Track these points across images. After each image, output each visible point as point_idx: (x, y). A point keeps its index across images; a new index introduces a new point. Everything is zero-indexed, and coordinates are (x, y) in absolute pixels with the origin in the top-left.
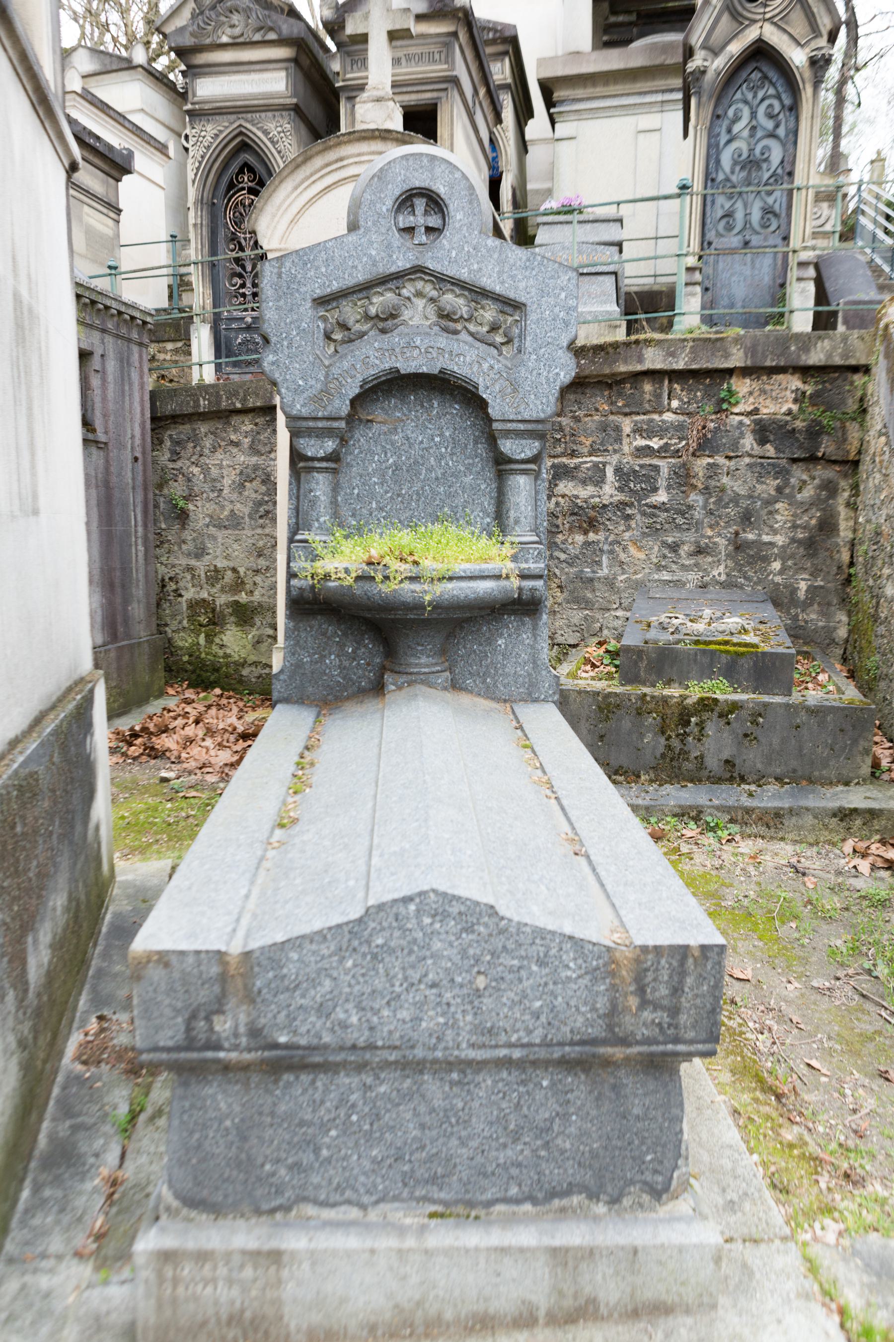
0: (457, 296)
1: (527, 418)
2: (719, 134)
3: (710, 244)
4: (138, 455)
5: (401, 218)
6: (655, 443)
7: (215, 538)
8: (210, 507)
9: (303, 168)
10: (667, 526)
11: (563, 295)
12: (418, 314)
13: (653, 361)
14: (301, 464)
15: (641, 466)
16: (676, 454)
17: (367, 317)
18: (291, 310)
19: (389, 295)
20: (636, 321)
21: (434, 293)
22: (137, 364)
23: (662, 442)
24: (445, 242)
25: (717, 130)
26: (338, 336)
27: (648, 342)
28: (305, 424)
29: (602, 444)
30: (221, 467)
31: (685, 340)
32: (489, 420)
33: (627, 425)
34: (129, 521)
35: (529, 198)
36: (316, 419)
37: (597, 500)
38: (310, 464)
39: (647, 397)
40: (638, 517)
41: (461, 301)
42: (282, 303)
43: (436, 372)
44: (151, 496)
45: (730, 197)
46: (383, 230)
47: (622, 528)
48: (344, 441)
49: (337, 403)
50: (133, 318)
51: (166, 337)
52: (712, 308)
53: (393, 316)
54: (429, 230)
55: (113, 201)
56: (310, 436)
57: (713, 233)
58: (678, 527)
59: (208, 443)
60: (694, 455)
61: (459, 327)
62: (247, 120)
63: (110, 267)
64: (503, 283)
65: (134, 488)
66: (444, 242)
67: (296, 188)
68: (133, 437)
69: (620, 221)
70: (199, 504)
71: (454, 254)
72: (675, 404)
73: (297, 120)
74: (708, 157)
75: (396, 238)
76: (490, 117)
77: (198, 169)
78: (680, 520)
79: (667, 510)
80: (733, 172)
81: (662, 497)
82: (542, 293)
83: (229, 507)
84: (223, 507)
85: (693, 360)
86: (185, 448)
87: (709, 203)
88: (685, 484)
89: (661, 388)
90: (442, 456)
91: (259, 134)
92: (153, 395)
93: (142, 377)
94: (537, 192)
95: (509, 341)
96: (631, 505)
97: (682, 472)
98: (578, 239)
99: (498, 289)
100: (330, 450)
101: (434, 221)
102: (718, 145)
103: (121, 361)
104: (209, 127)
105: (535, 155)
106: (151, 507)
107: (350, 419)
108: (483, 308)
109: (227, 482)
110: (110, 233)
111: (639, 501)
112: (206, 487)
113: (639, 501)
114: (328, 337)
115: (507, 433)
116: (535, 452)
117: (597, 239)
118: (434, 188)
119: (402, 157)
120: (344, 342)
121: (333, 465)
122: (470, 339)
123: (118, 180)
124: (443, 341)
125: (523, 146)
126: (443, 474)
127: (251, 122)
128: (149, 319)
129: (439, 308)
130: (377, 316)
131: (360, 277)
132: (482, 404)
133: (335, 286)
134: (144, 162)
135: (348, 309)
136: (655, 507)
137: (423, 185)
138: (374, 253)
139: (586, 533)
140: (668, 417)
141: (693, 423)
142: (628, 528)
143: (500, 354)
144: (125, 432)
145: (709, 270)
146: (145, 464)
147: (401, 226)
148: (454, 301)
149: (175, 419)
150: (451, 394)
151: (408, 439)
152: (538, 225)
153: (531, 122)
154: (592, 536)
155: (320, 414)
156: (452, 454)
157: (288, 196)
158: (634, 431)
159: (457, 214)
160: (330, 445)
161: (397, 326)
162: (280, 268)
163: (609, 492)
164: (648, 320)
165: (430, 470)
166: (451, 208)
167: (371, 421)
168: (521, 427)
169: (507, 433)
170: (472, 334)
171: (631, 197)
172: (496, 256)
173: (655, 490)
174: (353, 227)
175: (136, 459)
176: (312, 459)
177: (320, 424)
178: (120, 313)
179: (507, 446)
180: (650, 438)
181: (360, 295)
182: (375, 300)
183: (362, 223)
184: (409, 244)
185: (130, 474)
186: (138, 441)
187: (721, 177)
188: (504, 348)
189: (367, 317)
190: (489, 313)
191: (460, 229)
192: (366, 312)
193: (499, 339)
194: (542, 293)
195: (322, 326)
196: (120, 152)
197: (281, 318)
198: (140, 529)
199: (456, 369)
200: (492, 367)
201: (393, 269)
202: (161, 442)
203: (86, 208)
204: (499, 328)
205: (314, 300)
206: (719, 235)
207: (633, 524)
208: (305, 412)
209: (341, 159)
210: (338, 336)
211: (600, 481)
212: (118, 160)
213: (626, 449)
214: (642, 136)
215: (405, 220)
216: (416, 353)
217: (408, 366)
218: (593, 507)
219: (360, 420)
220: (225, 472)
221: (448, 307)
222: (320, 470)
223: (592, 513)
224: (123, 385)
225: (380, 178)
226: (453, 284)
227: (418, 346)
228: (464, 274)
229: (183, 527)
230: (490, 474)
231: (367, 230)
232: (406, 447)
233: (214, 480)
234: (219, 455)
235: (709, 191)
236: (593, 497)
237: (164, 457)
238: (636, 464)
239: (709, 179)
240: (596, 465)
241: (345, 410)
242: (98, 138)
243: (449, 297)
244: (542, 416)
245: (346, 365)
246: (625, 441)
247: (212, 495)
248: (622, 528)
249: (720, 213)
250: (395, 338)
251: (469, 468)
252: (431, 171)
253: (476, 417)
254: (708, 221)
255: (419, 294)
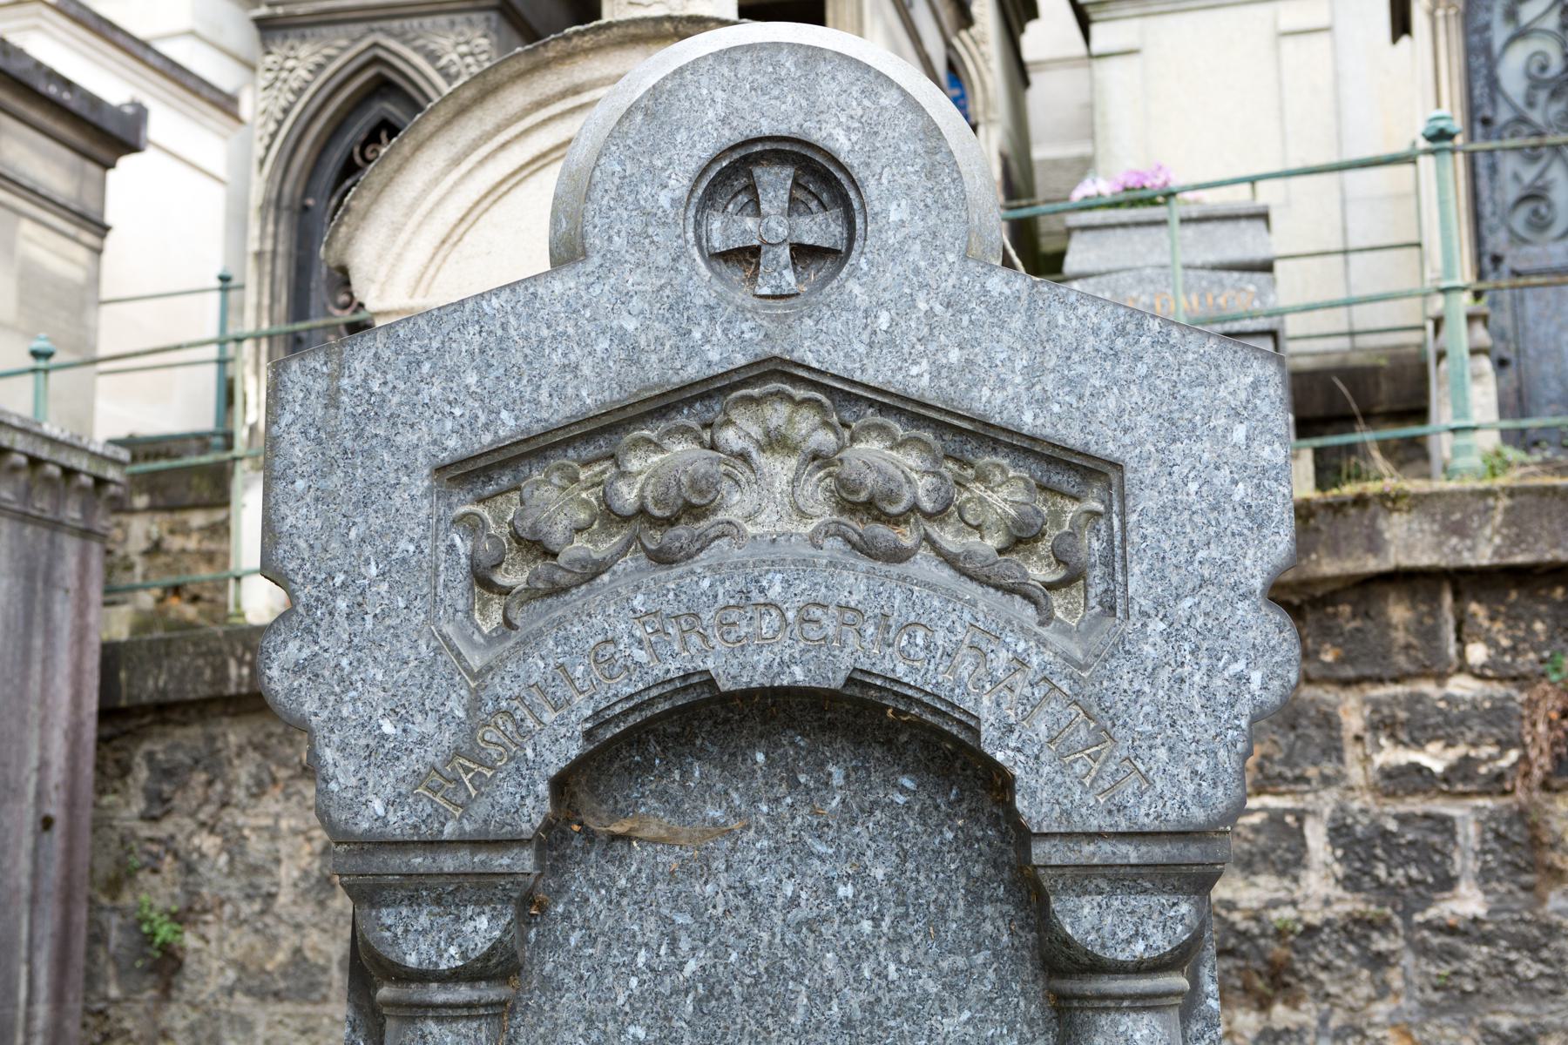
0: (898, 445)
1: (1149, 824)
2: (1487, 27)
3: (1497, 260)
4: (55, 810)
5: (716, 224)
6: (1435, 758)
7: (247, 1026)
8: (241, 941)
9: (478, 113)
10: (1491, 984)
11: (1240, 433)
12: (773, 502)
13: (1409, 549)
14: (385, 992)
15: (1403, 819)
16: (1497, 784)
17: (610, 516)
18: (365, 502)
19: (682, 449)
20: (1351, 449)
21: (825, 439)
22: (71, 582)
23: (1453, 755)
24: (854, 287)
25: (1482, 17)
26: (513, 577)
27: (1390, 501)
28: (396, 862)
29: (1288, 761)
30: (274, 834)
31: (1487, 493)
32: (1021, 836)
33: (1352, 712)
34: (12, 992)
35: (1039, 178)
36: (435, 844)
37: (1288, 913)
38: (415, 993)
39: (1400, 637)
40: (1408, 959)
41: (911, 460)
42: (337, 479)
43: (837, 682)
44: (81, 915)
45: (1531, 155)
46: (662, 259)
47: (1365, 990)
48: (529, 905)
49: (507, 792)
50: (69, 473)
51: (191, 498)
52: (1524, 413)
53: (692, 512)
54: (803, 254)
55: (91, 207)
56: (413, 900)
57: (1502, 236)
58: (1524, 986)
59: (244, 772)
60: (1545, 786)
61: (907, 537)
62: (390, 34)
63: (36, 354)
64: (1042, 402)
65: (33, 900)
66: (853, 286)
67: (456, 162)
68: (43, 766)
69: (1263, 216)
70: (212, 932)
71: (884, 321)
72: (1477, 653)
73: (506, 29)
74: (1469, 74)
75: (702, 281)
76: (947, 14)
77: (273, 136)
78: (1528, 968)
79: (1487, 940)
80: (1531, 104)
81: (1468, 902)
82: (1172, 429)
83: (289, 941)
84: (273, 942)
85: (1516, 542)
86: (184, 786)
87: (1483, 171)
88: (1532, 867)
89: (1435, 612)
90: (865, 948)
91: (418, 60)
92: (112, 655)
93: (82, 612)
94: (1056, 164)
95: (1073, 578)
96: (1385, 926)
97: (1517, 833)
98: (1182, 259)
99: (1028, 421)
100: (483, 946)
101: (818, 228)
102: (1487, 49)
103: (30, 576)
104: (304, 50)
105: (1042, 91)
106: (80, 945)
107: (552, 841)
108: (982, 477)
109: (287, 873)
110: (77, 274)
111: (1406, 915)
112: (233, 888)
113: (1406, 915)
114: (482, 579)
115: (1083, 877)
116: (1181, 933)
117: (1213, 258)
118: (816, 137)
119: (719, 56)
120: (532, 594)
121: (490, 992)
122: (945, 574)
123: (107, 166)
124: (855, 583)
125: (1019, 72)
126: (869, 1008)
127: (401, 36)
128: (112, 473)
129: (842, 483)
130: (642, 511)
131: (589, 397)
132: (998, 783)
133: (508, 425)
134: (168, 122)
135: (549, 493)
136: (1451, 930)
137: (783, 130)
138: (631, 325)
139: (1264, 1005)
140: (1462, 687)
141: (1532, 704)
142: (1383, 991)
143: (1046, 619)
144: (22, 755)
145: (1504, 319)
146: (71, 835)
147: (718, 244)
148: (889, 460)
149: (166, 712)
150: (889, 744)
151: (747, 893)
152: (1069, 232)
153: (1032, 28)
154: (1281, 1014)
155: (449, 830)
156: (896, 940)
157: (436, 181)
158: (1374, 727)
159: (891, 206)
160: (482, 929)
161: (706, 542)
162: (334, 377)
163: (1319, 889)
164: (1386, 448)
165: (823, 994)
166: (871, 190)
167: (626, 838)
168: (1131, 853)
169: (1083, 877)
170: (949, 560)
171: (1333, 159)
172: (1017, 323)
173: (1447, 883)
174: (567, 252)
175: (47, 823)
176: (422, 976)
177: (448, 862)
178: (35, 462)
179: (1085, 918)
180: (1417, 744)
181: (589, 451)
182: (634, 464)
183: (595, 240)
184: (742, 296)
185: (25, 864)
186: (56, 775)
187: (1504, 115)
188: (1057, 600)
189: (610, 516)
190: (1003, 494)
191: (902, 250)
192: (604, 500)
193: (1039, 572)
194: (1172, 429)
195: (463, 546)
196: (117, 112)
197: (329, 526)
198: (42, 1011)
199: (901, 670)
200: (1021, 663)
201: (693, 372)
202: (125, 770)
203: (26, 227)
204: (1039, 536)
205: (440, 470)
206: (1517, 240)
207: (1395, 978)
208: (398, 823)
209: (576, 90)
210: (513, 577)
211: (1291, 862)
212: (112, 126)
213: (1356, 774)
214: (1289, 44)
215: (724, 230)
216: (768, 623)
217: (737, 668)
218: (1280, 934)
219: (590, 836)
220: (284, 848)
221: (870, 479)
222: (446, 1013)
223: (1277, 951)
224: (28, 635)
225: (649, 115)
226: (883, 409)
227: (779, 591)
228: (918, 379)
229: (166, 993)
230: (1026, 1003)
231: (612, 261)
232: (741, 920)
233: (255, 869)
234: (271, 803)
235: (1479, 145)
236: (1275, 904)
237: (129, 809)
238: (1388, 814)
239: (1479, 120)
240: (1276, 817)
241: (534, 811)
242: (68, 84)
243: (871, 447)
244: (1199, 815)
245: (537, 667)
246: (1352, 753)
247: (247, 909)
248: (1365, 990)
249: (1512, 193)
250: (700, 579)
251: (954, 985)
252: (808, 90)
253: (972, 815)
254: (1487, 209)
255: (776, 442)
